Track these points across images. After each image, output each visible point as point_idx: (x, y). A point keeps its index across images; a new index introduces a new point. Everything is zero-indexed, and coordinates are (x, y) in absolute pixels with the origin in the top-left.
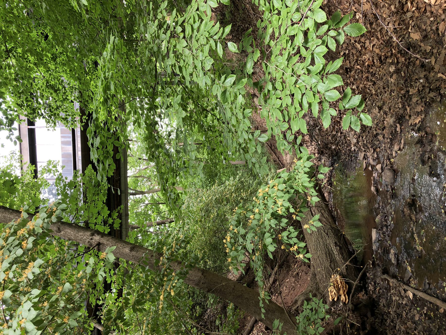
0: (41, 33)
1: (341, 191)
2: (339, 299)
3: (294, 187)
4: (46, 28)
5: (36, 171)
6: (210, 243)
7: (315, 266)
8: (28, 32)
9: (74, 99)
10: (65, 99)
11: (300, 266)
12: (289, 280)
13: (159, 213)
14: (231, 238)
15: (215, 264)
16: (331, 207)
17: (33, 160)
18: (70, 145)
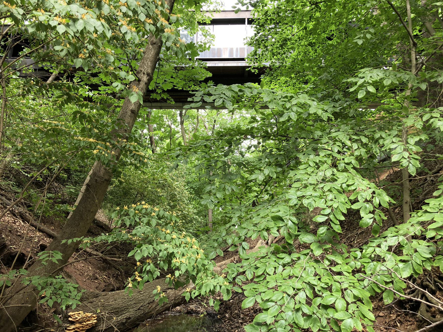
0: (333, 34)
1: (181, 324)
2: (72, 323)
3: (200, 275)
4: (338, 39)
5: (205, 24)
6: (131, 189)
7: (106, 296)
8: (335, 23)
9: (272, 62)
10: (274, 54)
11: (104, 281)
12: (90, 270)
13: (161, 139)
14: (146, 209)
15: (109, 194)
16: (165, 314)
17: (215, 22)
18: (230, 56)
